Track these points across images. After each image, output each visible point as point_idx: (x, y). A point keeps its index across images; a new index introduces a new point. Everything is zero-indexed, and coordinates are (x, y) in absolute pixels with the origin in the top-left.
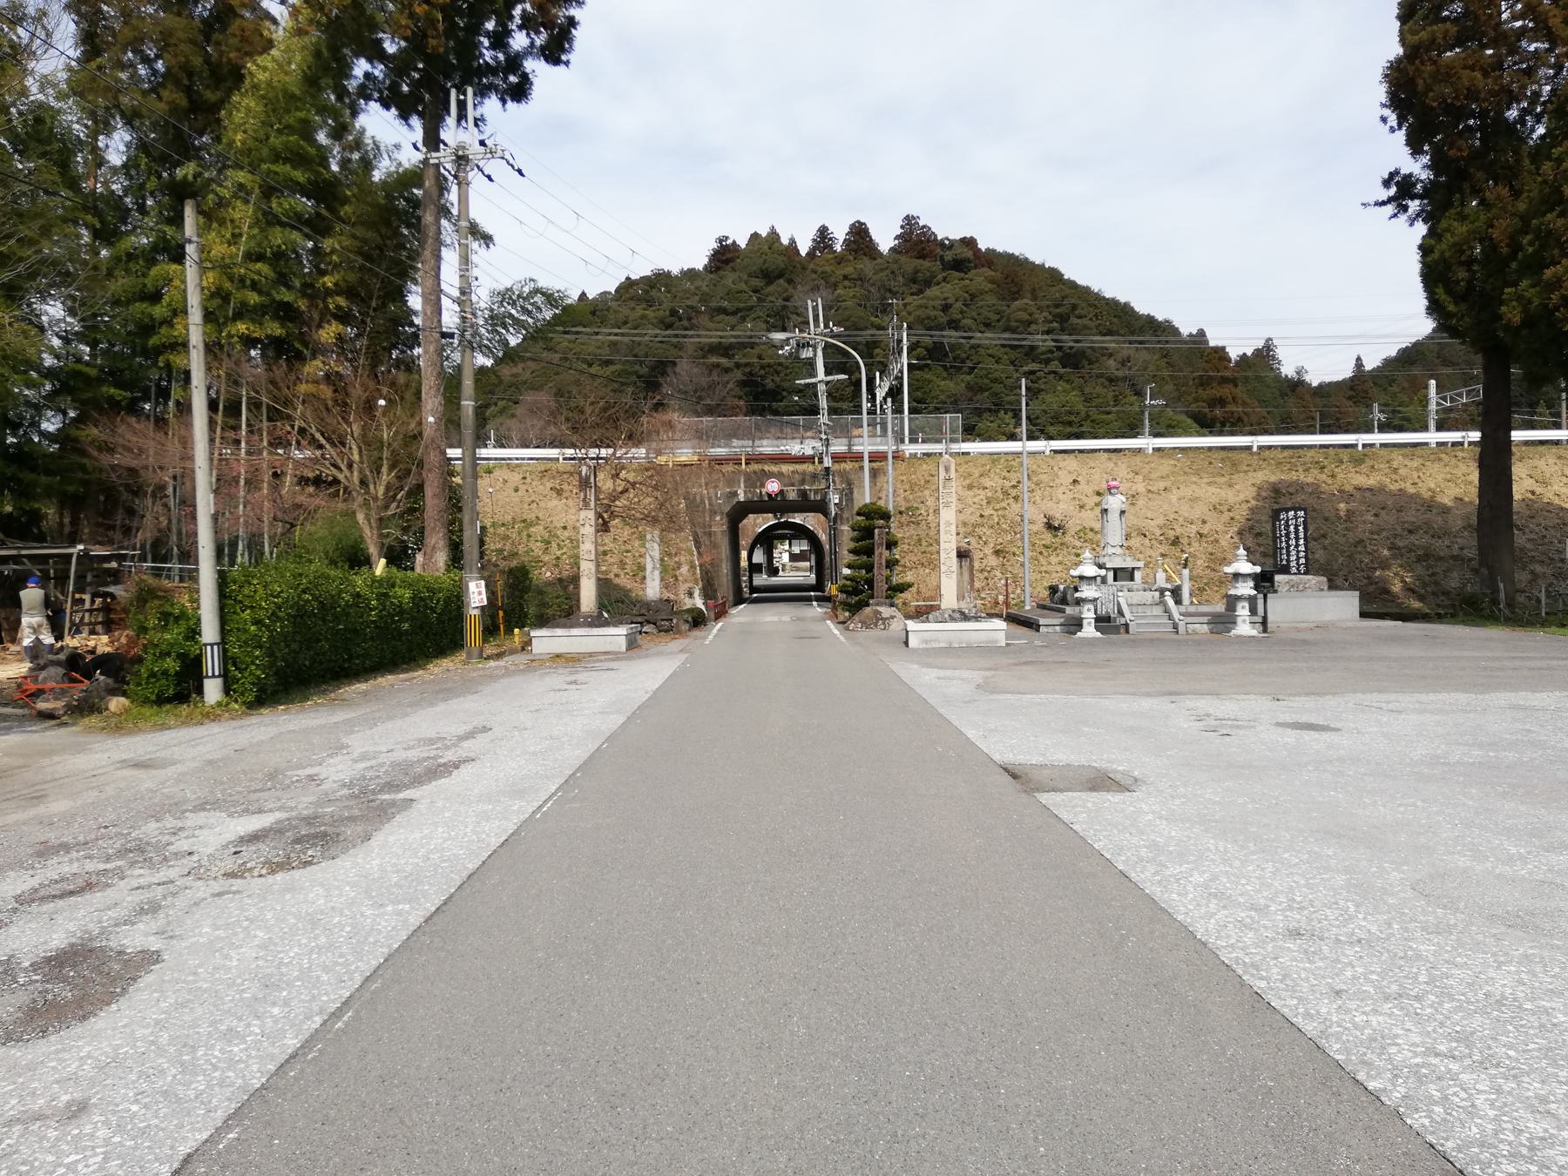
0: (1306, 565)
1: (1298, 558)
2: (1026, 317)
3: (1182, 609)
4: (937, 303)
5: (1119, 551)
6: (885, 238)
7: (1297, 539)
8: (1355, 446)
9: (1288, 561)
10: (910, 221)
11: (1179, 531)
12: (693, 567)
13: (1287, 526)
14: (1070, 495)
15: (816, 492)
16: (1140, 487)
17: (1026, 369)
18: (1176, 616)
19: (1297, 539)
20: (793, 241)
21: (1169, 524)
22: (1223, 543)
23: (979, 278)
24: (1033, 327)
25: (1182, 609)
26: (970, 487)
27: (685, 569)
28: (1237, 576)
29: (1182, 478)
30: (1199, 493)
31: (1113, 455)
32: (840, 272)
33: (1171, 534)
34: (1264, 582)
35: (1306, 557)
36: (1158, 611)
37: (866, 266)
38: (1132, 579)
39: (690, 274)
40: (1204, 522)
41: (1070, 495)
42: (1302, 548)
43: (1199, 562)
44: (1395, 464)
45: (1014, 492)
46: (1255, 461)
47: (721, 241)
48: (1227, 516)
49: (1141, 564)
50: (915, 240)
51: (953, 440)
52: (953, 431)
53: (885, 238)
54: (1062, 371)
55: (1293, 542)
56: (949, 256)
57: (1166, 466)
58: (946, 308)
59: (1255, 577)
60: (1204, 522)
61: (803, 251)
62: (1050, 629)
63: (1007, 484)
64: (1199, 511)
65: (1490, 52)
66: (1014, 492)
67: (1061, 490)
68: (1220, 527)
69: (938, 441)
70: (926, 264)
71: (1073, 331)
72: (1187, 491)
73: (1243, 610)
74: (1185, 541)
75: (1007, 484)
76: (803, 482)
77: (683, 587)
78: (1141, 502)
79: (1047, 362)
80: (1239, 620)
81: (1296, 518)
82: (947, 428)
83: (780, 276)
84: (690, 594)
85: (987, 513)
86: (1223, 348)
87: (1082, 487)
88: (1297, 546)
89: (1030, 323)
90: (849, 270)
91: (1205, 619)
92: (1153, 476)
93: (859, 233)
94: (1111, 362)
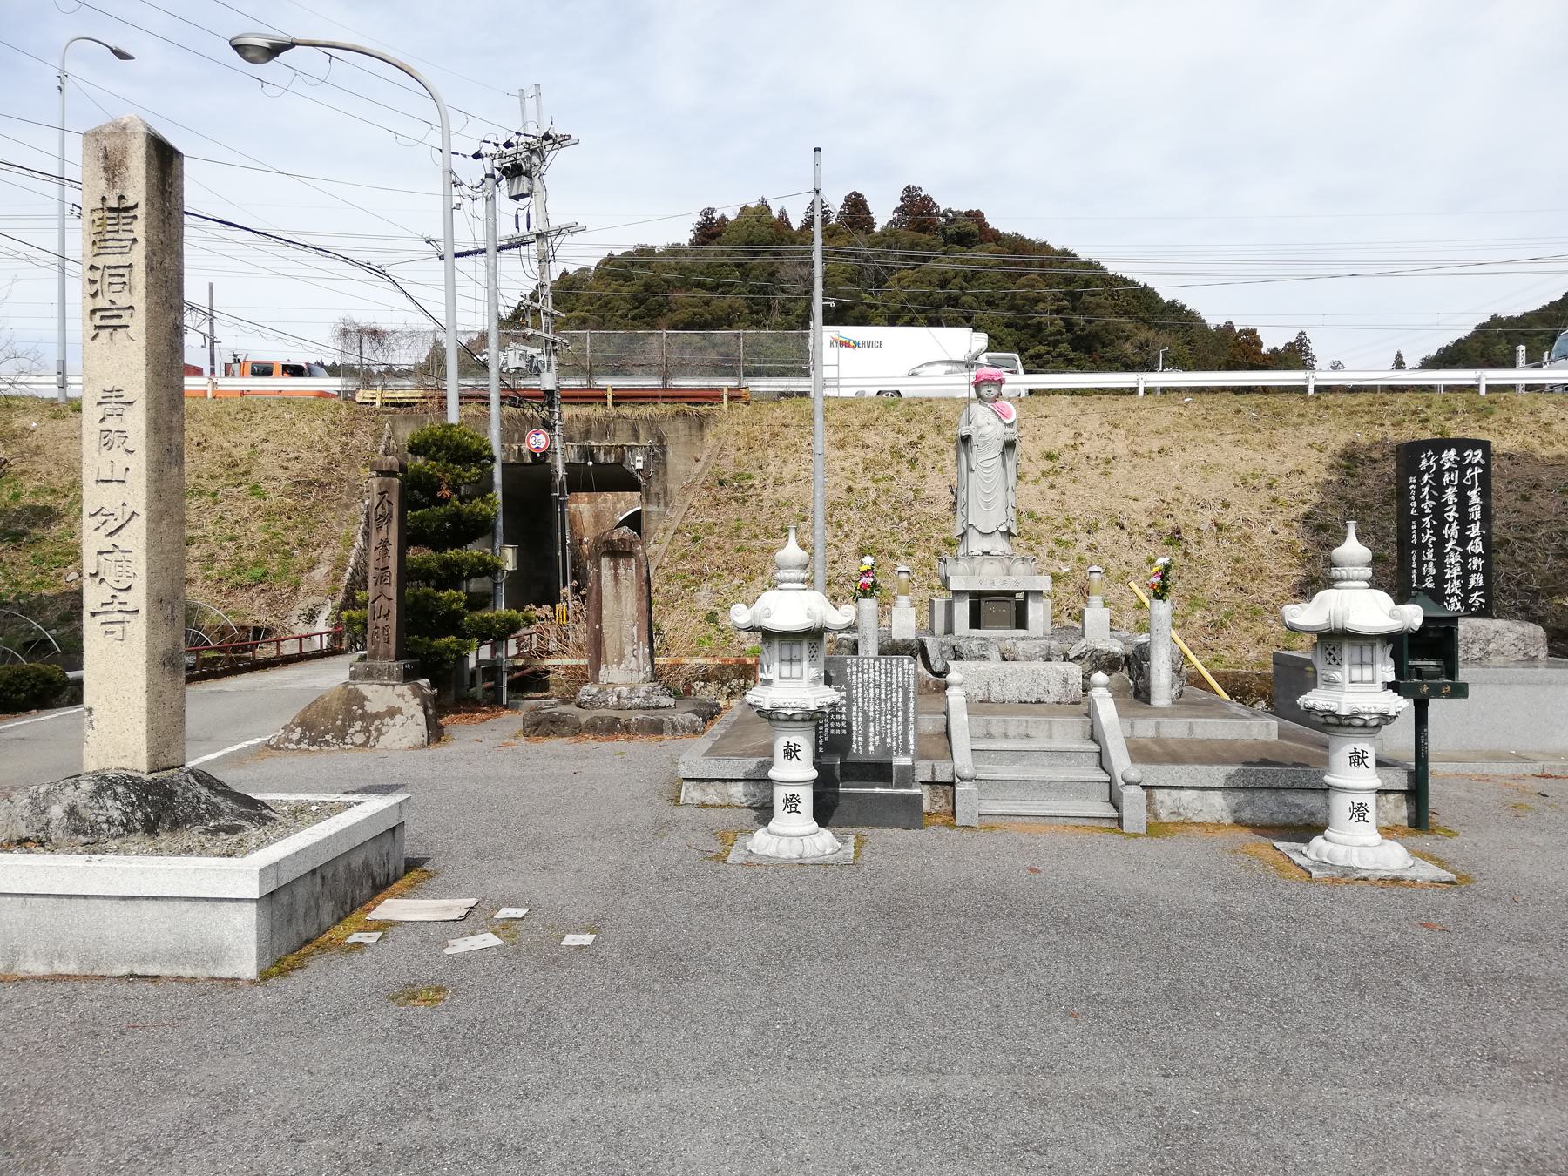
0: (1486, 590)
1: (1465, 574)
3: (1145, 728)
4: (934, 278)
5: (999, 545)
6: (883, 213)
7: (1464, 522)
8: (1475, 388)
9: (1440, 579)
10: (910, 192)
11: (1181, 518)
12: (340, 566)
13: (1440, 488)
15: (608, 451)
16: (1120, 446)
17: (1031, 352)
18: (1121, 762)
19: (1464, 522)
20: (783, 213)
21: (1165, 507)
22: (1259, 542)
23: (982, 255)
24: (1041, 305)
25: (1145, 728)
26: (842, 445)
28: (1334, 639)
30: (1217, 456)
31: (1077, 398)
33: (1168, 525)
34: (1425, 661)
35: (1486, 571)
36: (1067, 734)
37: (859, 238)
38: (1021, 622)
39: (675, 250)
40: (1226, 505)
42: (1476, 547)
43: (1215, 575)
44: (1545, 417)
45: (909, 453)
46: (1311, 408)
47: (706, 214)
48: (1264, 496)
49: (1043, 583)
50: (916, 208)
53: (883, 213)
54: (1072, 355)
55: (1453, 531)
56: (951, 230)
57: (1164, 414)
58: (943, 284)
59: (1401, 645)
60: (1226, 505)
62: (712, 794)
63: (903, 440)
64: (1218, 486)
66: (909, 453)
68: (1254, 514)
71: (1086, 310)
72: (1197, 455)
73: (1354, 776)
74: (1191, 536)
76: (587, 434)
77: (303, 604)
78: (1119, 471)
79: (1056, 344)
80: (1341, 805)
81: (1462, 467)
84: (311, 616)
86: (1253, 332)
88: (1463, 540)
91: (1218, 774)
92: (1142, 430)
93: (856, 206)
94: (1127, 345)
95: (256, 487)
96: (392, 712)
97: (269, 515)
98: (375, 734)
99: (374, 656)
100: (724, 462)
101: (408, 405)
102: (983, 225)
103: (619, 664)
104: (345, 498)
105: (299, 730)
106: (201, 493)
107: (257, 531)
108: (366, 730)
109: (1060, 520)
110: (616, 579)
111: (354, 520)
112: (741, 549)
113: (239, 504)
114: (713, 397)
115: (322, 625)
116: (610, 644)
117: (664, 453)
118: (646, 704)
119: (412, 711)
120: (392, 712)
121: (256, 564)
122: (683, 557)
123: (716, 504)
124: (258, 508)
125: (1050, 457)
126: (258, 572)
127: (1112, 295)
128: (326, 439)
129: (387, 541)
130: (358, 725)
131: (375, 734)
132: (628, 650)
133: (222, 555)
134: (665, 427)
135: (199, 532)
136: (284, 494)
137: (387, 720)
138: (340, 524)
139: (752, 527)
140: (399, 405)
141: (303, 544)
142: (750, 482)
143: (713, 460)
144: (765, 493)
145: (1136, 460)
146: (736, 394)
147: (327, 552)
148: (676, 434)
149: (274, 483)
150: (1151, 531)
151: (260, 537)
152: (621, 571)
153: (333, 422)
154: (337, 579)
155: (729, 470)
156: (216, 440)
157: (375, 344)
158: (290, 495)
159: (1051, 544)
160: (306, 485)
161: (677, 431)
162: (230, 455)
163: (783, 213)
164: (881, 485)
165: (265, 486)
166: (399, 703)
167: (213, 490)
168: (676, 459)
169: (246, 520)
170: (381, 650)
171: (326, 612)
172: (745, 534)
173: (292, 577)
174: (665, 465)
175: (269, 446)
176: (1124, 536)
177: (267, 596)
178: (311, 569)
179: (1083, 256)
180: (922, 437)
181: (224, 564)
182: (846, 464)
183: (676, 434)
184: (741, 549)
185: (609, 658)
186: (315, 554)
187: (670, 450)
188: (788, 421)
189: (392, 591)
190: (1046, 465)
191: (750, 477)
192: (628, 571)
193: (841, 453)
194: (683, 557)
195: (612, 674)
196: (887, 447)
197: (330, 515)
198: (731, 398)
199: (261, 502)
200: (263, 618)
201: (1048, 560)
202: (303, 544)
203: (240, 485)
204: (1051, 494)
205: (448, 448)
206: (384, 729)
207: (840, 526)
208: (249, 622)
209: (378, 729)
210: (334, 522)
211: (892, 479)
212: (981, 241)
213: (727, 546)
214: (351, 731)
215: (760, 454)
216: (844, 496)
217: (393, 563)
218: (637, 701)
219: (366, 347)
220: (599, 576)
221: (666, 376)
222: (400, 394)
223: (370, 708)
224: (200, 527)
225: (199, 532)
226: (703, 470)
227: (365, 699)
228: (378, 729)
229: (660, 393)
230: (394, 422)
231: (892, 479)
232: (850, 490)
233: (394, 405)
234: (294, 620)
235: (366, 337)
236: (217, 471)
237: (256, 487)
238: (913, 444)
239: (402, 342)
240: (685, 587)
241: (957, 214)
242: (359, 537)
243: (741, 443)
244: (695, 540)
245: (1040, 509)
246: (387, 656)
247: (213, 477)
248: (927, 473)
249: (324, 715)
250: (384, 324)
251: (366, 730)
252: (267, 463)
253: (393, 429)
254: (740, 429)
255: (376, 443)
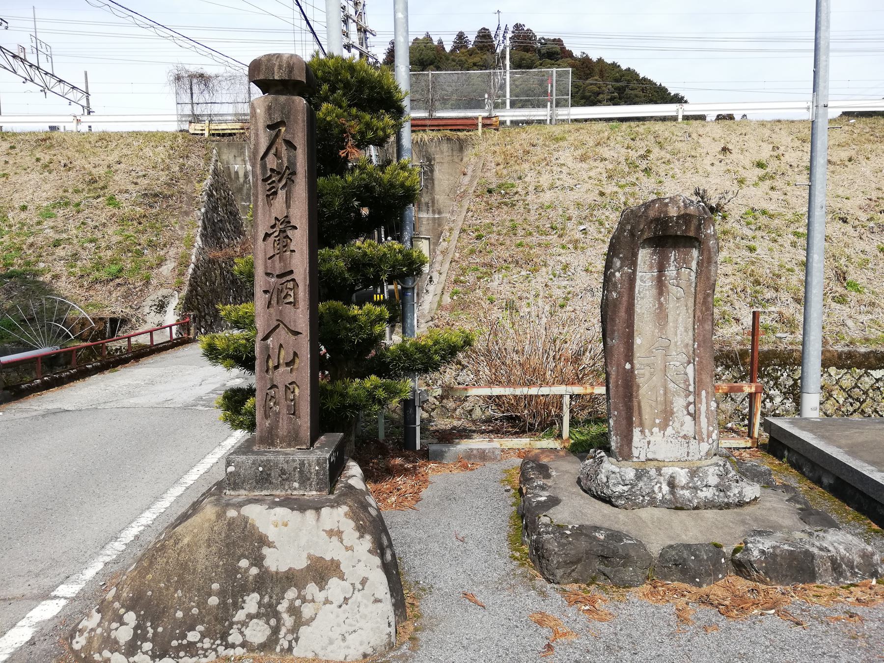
2: (596, 89)
12: (183, 263)
14: (722, 167)
20: (441, 42)
24: (601, 96)
26: (583, 159)
27: (167, 269)
29: (869, 146)
32: (471, 61)
41: (722, 167)
45: (644, 165)
51: (558, 104)
52: (560, 92)
61: (448, 48)
63: (633, 155)
65: (178, 631)
67: (708, 161)
69: (542, 105)
70: (528, 55)
75: (633, 155)
77: (154, 296)
82: (552, 88)
83: (431, 63)
84: (161, 307)
85: (609, 189)
87: (735, 156)
89: (599, 94)
90: (476, 59)
95: (112, 198)
96: (321, 571)
97: (123, 221)
98: (288, 620)
99: (269, 439)
100: (488, 174)
101: (230, 135)
102: (563, 49)
103: (664, 426)
104: (185, 207)
105: (131, 618)
106: (67, 204)
107: (113, 234)
108: (269, 612)
109: (789, 216)
110: (660, 285)
111: (194, 225)
112: (520, 245)
113: (98, 212)
114: (470, 125)
115: (171, 317)
116: (648, 393)
117: (432, 171)
118: (723, 499)
119: (362, 571)
120: (321, 571)
121: (113, 261)
122: (472, 252)
123: (490, 208)
124: (114, 215)
125: (760, 165)
126: (114, 268)
127: (643, 90)
128: (167, 161)
129: (287, 221)
130: (251, 603)
131: (288, 620)
132: (679, 403)
133: (84, 254)
134: (432, 149)
135: (65, 236)
136: (135, 204)
137: (312, 589)
138: (182, 228)
139: (525, 226)
140: (224, 135)
141: (151, 245)
142: (515, 190)
143: (479, 174)
144: (529, 198)
145: (832, 168)
146: (488, 122)
147: (172, 252)
148: (442, 155)
149: (126, 195)
150: (872, 224)
151: (115, 239)
152: (671, 271)
153: (172, 148)
154: (181, 274)
155: (494, 183)
156: (79, 162)
157: (202, 87)
158: (140, 205)
159: (791, 237)
160: (152, 197)
161: (442, 153)
162: (90, 174)
163: (441, 42)
164: (627, 189)
165: (119, 197)
166: (331, 551)
167: (76, 201)
168: (442, 176)
169: (104, 225)
170: (283, 428)
171: (174, 303)
172: (520, 232)
173: (144, 272)
174: (433, 180)
175: (122, 166)
176: (848, 228)
177: (123, 289)
178: (159, 265)
179: (624, 67)
180: (649, 151)
181: (86, 262)
182: (592, 174)
183: (442, 155)
184: (520, 245)
185: (646, 416)
186: (162, 253)
187: (437, 168)
188: (535, 142)
189: (301, 318)
190: (761, 172)
191: (513, 186)
192: (682, 271)
193: (584, 165)
194: (472, 252)
195: (654, 444)
196: (622, 159)
197: (173, 221)
198: (484, 126)
199: (116, 211)
200: (116, 308)
201: (793, 250)
202: (151, 245)
203: (99, 197)
204: (774, 195)
205: (347, 85)
206: (307, 611)
207: (601, 224)
208: (107, 314)
209: (294, 611)
210: (177, 227)
211: (634, 184)
212: (562, 58)
213: (508, 242)
214: (240, 616)
215: (517, 167)
216: (599, 198)
217: (299, 263)
218: (707, 494)
219: (195, 88)
220: (631, 280)
221: (431, 108)
222: (224, 126)
223: (276, 561)
224: (66, 231)
225: (65, 236)
226: (471, 181)
227: (263, 541)
228: (294, 611)
229: (428, 122)
230: (220, 149)
231: (634, 184)
232: (602, 194)
233: (219, 135)
234: (147, 310)
235: (195, 81)
236: (80, 187)
237: (112, 198)
238: (644, 157)
239: (224, 84)
240: (479, 278)
241: (549, 40)
242: (198, 239)
243: (500, 159)
244: (479, 238)
245: (771, 207)
246: (293, 439)
247: (77, 191)
248: (663, 179)
249: (181, 583)
250: (209, 71)
251: (269, 612)
252: (121, 180)
253: (219, 154)
254: (497, 148)
255: (207, 164)
